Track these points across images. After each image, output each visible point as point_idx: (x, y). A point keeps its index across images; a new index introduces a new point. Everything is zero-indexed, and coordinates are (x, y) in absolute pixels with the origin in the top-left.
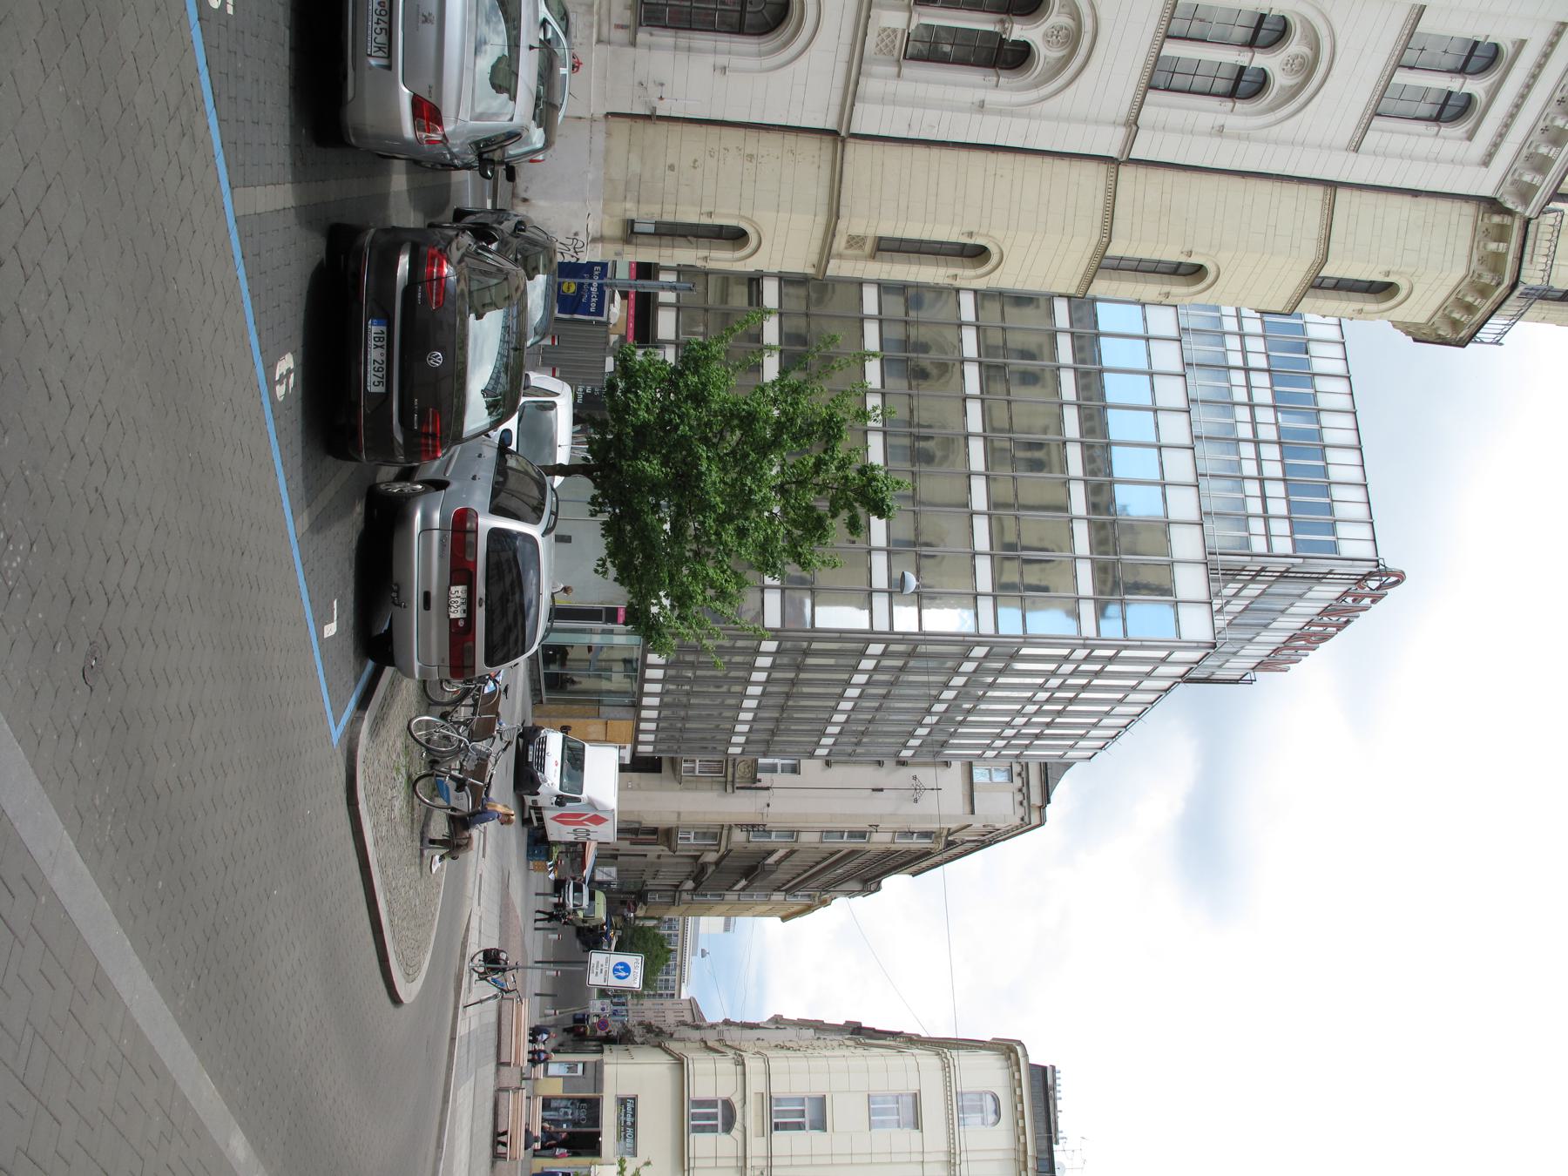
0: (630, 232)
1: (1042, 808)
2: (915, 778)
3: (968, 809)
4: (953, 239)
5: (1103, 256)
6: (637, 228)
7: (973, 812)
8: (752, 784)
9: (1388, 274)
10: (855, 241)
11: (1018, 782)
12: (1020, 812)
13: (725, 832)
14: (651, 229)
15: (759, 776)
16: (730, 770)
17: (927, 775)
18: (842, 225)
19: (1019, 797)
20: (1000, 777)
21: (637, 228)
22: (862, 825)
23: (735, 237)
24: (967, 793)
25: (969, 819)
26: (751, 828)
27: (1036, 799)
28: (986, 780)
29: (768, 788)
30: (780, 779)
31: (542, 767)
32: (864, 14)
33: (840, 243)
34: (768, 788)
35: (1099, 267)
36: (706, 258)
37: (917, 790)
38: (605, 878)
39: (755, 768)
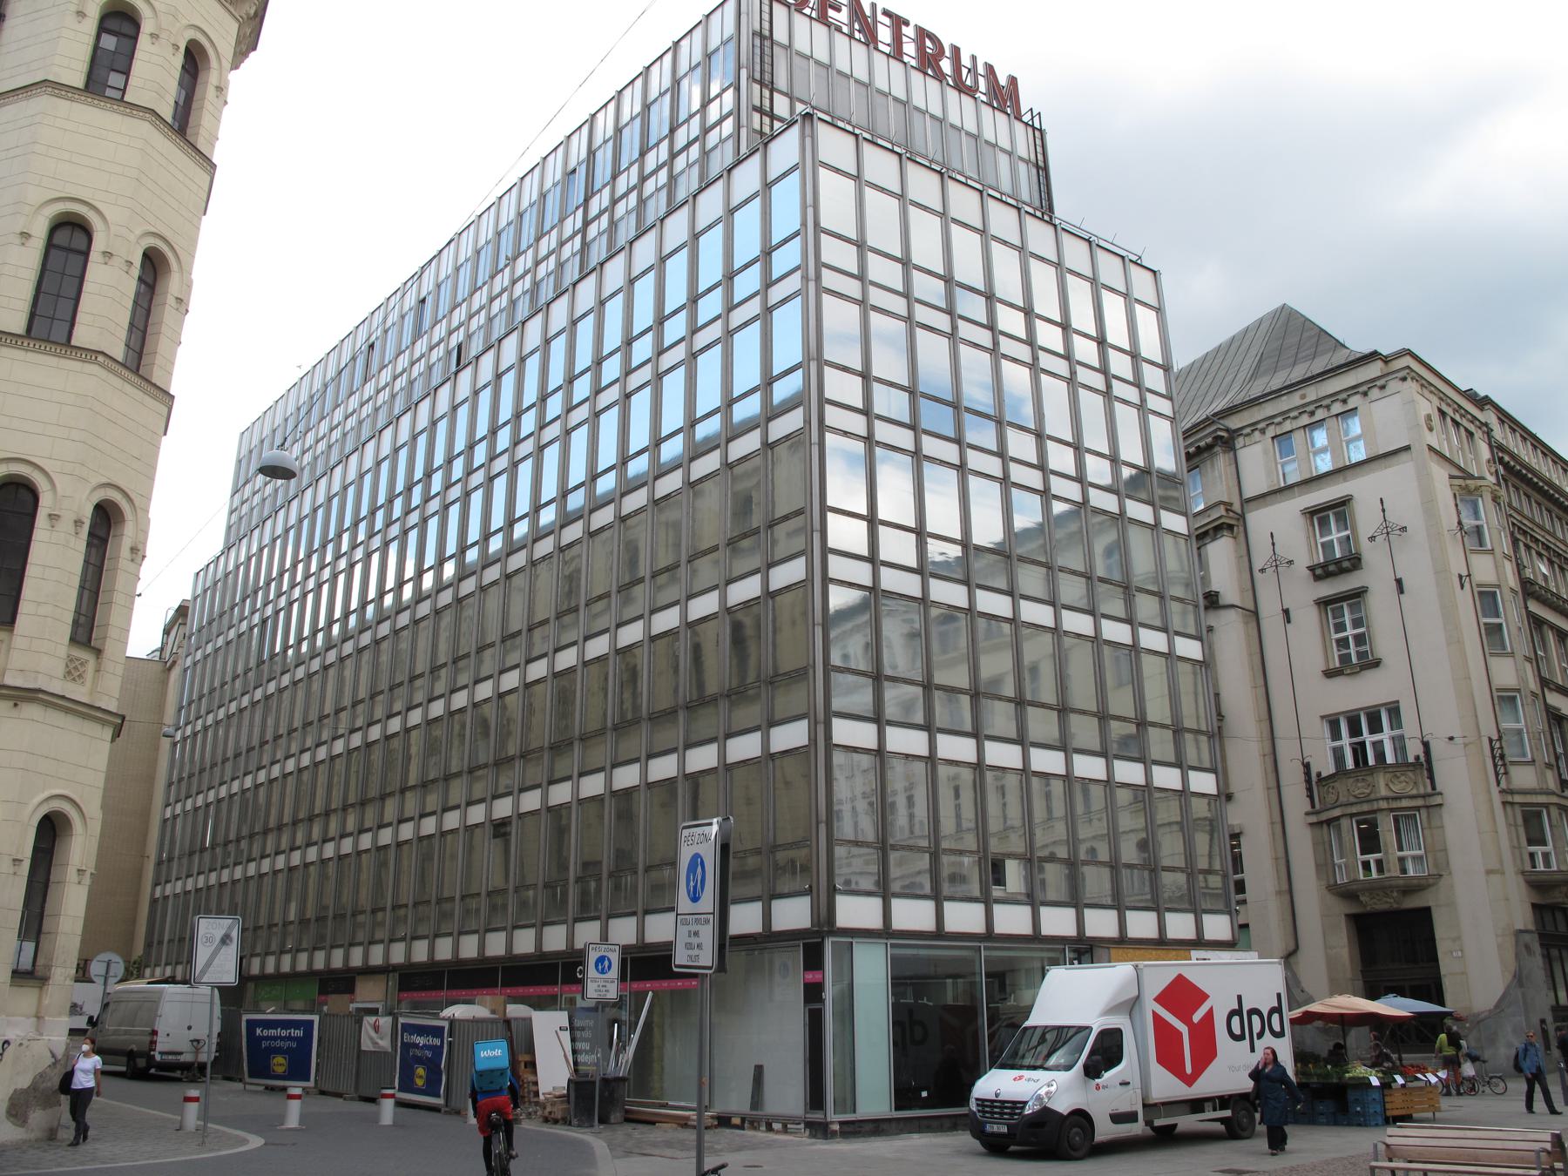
0: (28, 976)
1: (1386, 360)
2: (1372, 538)
3: (1404, 456)
4: (82, 546)
5: (123, 365)
6: (26, 963)
7: (1407, 448)
8: (1425, 765)
9: (176, 47)
10: (73, 672)
11: (1354, 401)
12: (1394, 385)
13: (1518, 799)
14: (29, 947)
15: (1411, 759)
16: (1405, 803)
17: (1366, 519)
18: (56, 687)
19: (1375, 393)
20: (1355, 426)
21: (26, 963)
22: (1465, 601)
23: (51, 830)
24: (1383, 462)
25: (1420, 450)
26: (1500, 761)
27: (1375, 369)
28: (1361, 444)
29: (1426, 745)
30: (1409, 728)
31: (1018, 1105)
32: (99, 714)
33: (79, 692)
34: (1426, 745)
35: (136, 371)
36: (80, 872)
37: (1390, 531)
38: (202, 954)
39: (1403, 766)
